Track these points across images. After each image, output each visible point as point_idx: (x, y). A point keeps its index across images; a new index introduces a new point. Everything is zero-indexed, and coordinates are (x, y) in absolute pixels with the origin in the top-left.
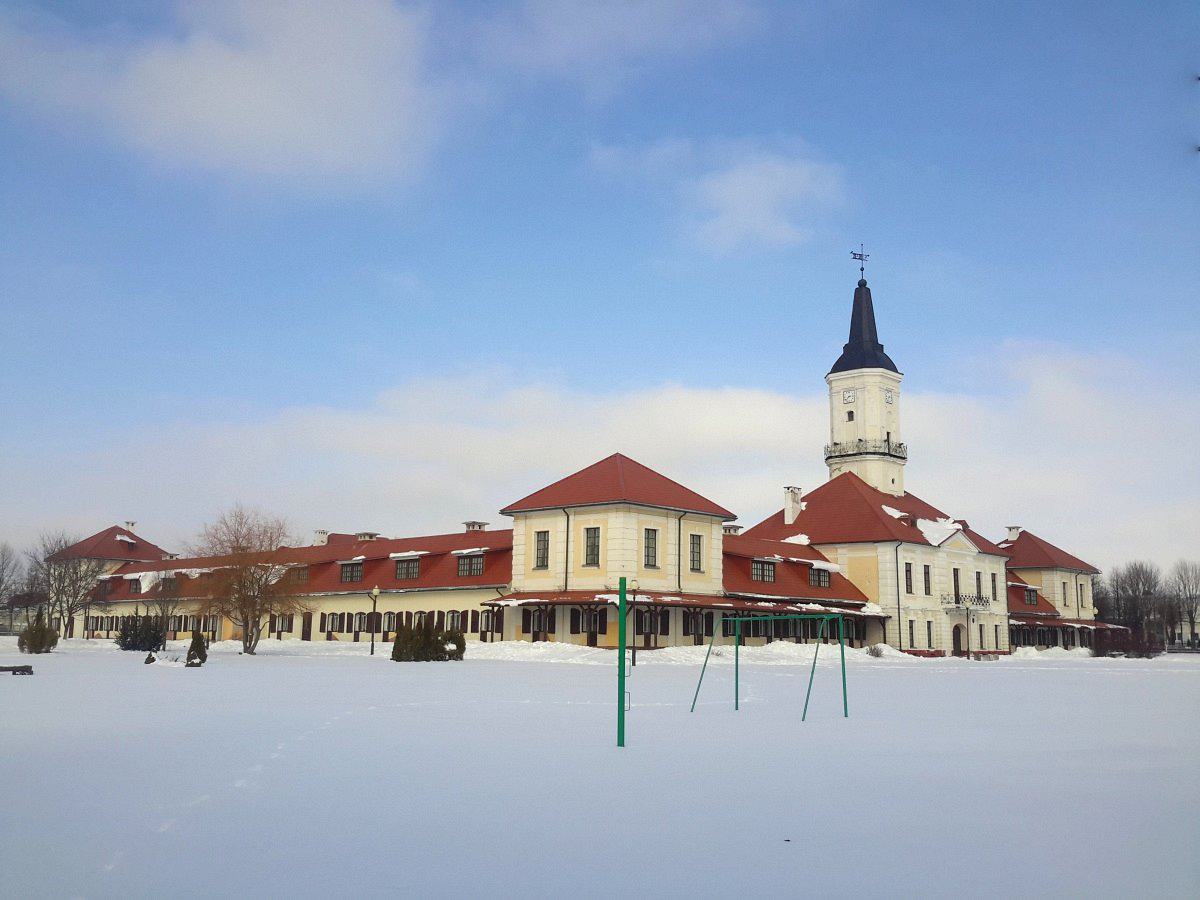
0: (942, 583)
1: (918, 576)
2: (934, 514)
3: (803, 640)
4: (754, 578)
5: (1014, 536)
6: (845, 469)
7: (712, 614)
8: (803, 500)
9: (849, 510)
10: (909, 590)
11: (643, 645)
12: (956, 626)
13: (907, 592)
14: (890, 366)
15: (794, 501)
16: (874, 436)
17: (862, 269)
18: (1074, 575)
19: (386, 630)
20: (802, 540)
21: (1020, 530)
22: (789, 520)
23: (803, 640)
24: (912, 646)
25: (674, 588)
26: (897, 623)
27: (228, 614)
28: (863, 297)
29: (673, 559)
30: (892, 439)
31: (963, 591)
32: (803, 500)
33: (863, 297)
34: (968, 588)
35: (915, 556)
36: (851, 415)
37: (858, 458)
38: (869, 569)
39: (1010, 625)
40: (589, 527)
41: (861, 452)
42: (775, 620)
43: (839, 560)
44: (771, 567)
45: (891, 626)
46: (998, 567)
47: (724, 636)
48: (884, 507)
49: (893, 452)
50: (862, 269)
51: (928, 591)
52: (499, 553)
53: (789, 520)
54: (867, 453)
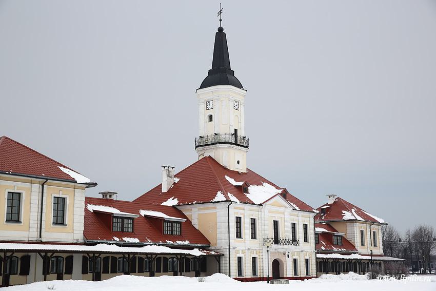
1: (311, 236)
2: (259, 180)
3: (179, 273)
5: (331, 201)
6: (207, 155)
8: (175, 176)
9: (204, 179)
10: (239, 235)
12: (275, 260)
13: (237, 237)
14: (205, 84)
15: (168, 176)
16: (225, 132)
17: (221, 20)
18: (368, 226)
19: (8, 272)
20: (172, 202)
21: (336, 197)
22: (164, 190)
23: (179, 273)
24: (295, 273)
25: (34, 236)
26: (228, 259)
27: (48, 257)
28: (220, 37)
29: (35, 215)
30: (239, 134)
31: (281, 236)
32: (175, 176)
33: (220, 37)
34: (285, 232)
35: (246, 212)
36: (211, 118)
37: (214, 146)
38: (215, 218)
39: (317, 258)
40: (58, 196)
41: (217, 142)
42: (139, 257)
43: (196, 214)
44: (178, 225)
45: (224, 261)
46: (308, 219)
47: (83, 273)
48: (226, 176)
50: (221, 20)
51: (254, 236)
53: (164, 190)
54: (220, 143)
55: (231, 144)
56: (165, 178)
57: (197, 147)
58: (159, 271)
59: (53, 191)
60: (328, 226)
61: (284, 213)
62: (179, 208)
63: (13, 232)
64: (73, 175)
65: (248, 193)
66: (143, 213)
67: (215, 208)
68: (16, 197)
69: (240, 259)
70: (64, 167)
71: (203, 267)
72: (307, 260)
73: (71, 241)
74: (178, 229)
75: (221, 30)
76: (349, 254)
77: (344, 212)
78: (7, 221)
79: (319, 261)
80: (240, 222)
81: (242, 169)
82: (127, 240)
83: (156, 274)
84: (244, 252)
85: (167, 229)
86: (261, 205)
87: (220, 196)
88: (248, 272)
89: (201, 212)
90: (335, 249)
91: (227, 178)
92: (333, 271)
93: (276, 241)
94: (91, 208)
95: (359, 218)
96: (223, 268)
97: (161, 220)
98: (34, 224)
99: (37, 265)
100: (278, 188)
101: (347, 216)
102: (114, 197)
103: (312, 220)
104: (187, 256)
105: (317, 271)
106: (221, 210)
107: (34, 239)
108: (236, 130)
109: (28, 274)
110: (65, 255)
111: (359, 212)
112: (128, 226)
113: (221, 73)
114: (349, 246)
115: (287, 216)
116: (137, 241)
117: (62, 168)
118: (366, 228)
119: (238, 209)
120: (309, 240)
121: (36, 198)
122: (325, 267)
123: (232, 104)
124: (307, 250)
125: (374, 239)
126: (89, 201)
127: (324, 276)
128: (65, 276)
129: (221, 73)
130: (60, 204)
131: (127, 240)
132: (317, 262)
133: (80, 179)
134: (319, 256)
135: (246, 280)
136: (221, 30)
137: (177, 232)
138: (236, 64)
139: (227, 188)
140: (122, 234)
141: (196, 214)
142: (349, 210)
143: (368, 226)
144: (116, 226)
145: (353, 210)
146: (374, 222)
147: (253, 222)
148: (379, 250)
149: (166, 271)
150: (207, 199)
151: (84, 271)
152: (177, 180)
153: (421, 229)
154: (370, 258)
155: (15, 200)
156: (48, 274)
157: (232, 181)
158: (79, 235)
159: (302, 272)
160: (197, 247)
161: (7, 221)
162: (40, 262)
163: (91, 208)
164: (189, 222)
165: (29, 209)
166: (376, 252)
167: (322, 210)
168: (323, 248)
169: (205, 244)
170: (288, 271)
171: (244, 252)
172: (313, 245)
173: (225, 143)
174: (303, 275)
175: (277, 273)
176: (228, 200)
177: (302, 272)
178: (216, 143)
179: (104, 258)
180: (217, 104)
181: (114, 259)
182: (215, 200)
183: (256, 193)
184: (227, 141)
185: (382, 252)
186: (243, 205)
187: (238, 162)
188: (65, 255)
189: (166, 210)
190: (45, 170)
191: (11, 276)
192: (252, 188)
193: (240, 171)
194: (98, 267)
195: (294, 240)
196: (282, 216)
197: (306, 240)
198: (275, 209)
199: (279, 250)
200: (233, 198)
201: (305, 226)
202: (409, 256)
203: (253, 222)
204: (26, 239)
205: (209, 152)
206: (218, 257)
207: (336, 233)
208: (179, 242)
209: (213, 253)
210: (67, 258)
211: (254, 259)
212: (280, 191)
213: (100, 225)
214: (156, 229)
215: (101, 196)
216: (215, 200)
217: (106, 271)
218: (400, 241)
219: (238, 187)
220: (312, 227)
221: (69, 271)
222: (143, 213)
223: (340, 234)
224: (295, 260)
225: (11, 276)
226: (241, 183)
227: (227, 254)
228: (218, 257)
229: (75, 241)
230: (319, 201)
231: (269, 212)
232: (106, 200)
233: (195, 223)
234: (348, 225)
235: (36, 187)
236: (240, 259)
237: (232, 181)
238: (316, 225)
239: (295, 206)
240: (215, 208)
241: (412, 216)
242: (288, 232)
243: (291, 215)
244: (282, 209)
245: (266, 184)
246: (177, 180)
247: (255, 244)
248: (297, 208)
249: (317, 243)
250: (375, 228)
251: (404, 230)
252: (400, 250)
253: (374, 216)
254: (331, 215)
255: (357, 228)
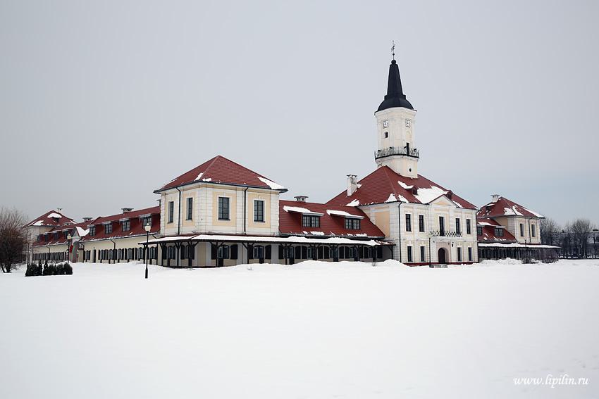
0: (432, 224)
2: (427, 184)
4: (347, 227)
6: (384, 165)
7: (271, 246)
9: (381, 184)
10: (409, 229)
11: (187, 265)
14: (410, 107)
15: (352, 182)
16: (399, 146)
17: (394, 54)
18: (527, 220)
20: (355, 203)
21: (499, 197)
22: (349, 194)
24: (423, 258)
25: (240, 231)
28: (394, 69)
31: (446, 229)
33: (394, 69)
34: (450, 226)
35: (415, 211)
36: (387, 134)
38: (389, 215)
40: (258, 200)
43: (373, 212)
44: (317, 219)
45: (396, 250)
46: (472, 215)
47: (280, 258)
49: (409, 152)
50: (394, 54)
51: (422, 229)
52: (155, 217)
53: (349, 194)
55: (404, 155)
56: (350, 184)
57: (376, 159)
58: (342, 257)
59: (254, 195)
60: (492, 221)
61: (448, 211)
62: (360, 208)
63: (224, 227)
64: (268, 183)
65: (417, 194)
66: (329, 212)
67: (388, 207)
68: (260, 204)
69: (409, 248)
70: (263, 177)
71: (381, 253)
72: (470, 249)
73: (269, 234)
74: (317, 222)
75: (394, 62)
76: (510, 243)
77: (505, 209)
78: (219, 219)
79: (482, 249)
80: (423, 220)
81: (413, 175)
82: (314, 233)
83: (265, 260)
84: (413, 242)
85: (348, 225)
86: (427, 204)
87: (392, 198)
88: (416, 257)
89: (376, 211)
90: (496, 239)
91: (400, 183)
92: (494, 257)
93: (442, 233)
94: (286, 208)
95: (519, 214)
96: (395, 255)
97: (343, 217)
98: (240, 221)
99: (243, 252)
100: (445, 190)
101: (508, 212)
102: (307, 201)
103: (474, 217)
104: (224, 243)
105: (479, 257)
106: (393, 209)
107: (240, 233)
108: (408, 144)
109: (270, 258)
110: (230, 244)
111: (520, 208)
112: (315, 223)
113: (395, 97)
114: (510, 237)
115: (452, 213)
116: (322, 234)
117: (260, 178)
118: (525, 222)
119: (407, 208)
120: (425, 230)
121: (240, 201)
122: (485, 254)
123: (404, 122)
124: (469, 241)
125: (533, 230)
126: (282, 203)
127: (485, 261)
128: (265, 260)
129: (395, 97)
130: (259, 206)
131: (314, 233)
132: (478, 250)
133: (274, 186)
134: (480, 245)
135: (415, 264)
136: (394, 62)
137: (356, 226)
138: (406, 90)
139: (399, 191)
140: (310, 229)
141: (373, 212)
142: (510, 207)
143: (527, 220)
144: (306, 222)
145: (514, 208)
146: (532, 216)
147: (421, 218)
148: (537, 239)
149: (305, 258)
150: (382, 200)
151: (281, 257)
152: (359, 186)
153: (578, 222)
154: (524, 246)
155: (224, 203)
156: (252, 258)
157: (404, 185)
158: (275, 230)
159: (465, 257)
160: (373, 239)
161: (219, 219)
162: (246, 251)
163: (286, 208)
164: (367, 219)
165: (235, 210)
166: (533, 241)
167: (487, 208)
168: (486, 239)
169: (380, 235)
170: (453, 256)
171: (413, 242)
172: (475, 237)
173: (398, 155)
174: (467, 260)
175: (443, 258)
176: (398, 201)
177: (465, 257)
178: (391, 155)
179: (232, 246)
180: (391, 123)
181: (305, 248)
182: (388, 201)
183: (423, 195)
184: (400, 152)
185: (540, 241)
186: (412, 205)
187: (410, 170)
188: (230, 244)
189: (350, 210)
190: (247, 179)
191: (224, 260)
192: (420, 191)
193: (412, 177)
194: (291, 254)
195: (458, 232)
196: (412, 210)
197: (469, 232)
198: (441, 207)
199: (445, 241)
200: (402, 199)
201: (468, 222)
202: (566, 245)
203: (421, 218)
204: (234, 233)
205: (387, 163)
206: (391, 247)
207: (497, 226)
208: (358, 235)
209: (386, 243)
210: (267, 247)
211: (422, 248)
212: (446, 193)
213: (292, 221)
214: (339, 224)
215: (296, 200)
216: (388, 201)
217: (298, 257)
218: (563, 232)
219: (408, 190)
220: (475, 221)
221: (269, 257)
222: (329, 212)
223: (502, 227)
224: (459, 249)
225: (224, 260)
226: (411, 187)
227: (398, 244)
228: (391, 247)
229: (272, 234)
230: (482, 200)
231: (436, 210)
232: (300, 202)
233: (373, 220)
234: (509, 219)
235: (240, 193)
236: (409, 248)
237: (404, 185)
238: (478, 220)
239: (459, 205)
240: (369, 209)
241: (575, 208)
242: (452, 226)
243: (455, 212)
244: (448, 207)
245: (434, 187)
246: (359, 186)
247: (423, 237)
248: (461, 206)
249: (480, 235)
250: (533, 221)
251: (562, 222)
252: (560, 240)
253: (536, 212)
254: (495, 210)
255: (517, 223)
